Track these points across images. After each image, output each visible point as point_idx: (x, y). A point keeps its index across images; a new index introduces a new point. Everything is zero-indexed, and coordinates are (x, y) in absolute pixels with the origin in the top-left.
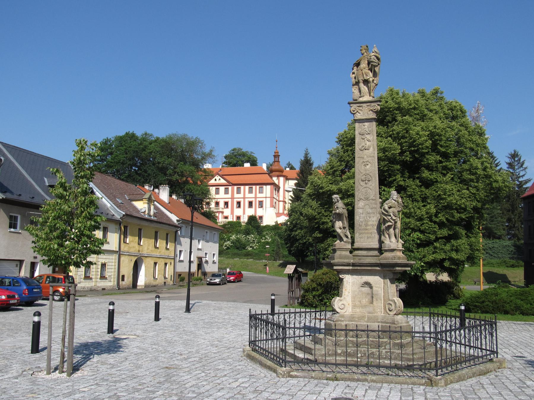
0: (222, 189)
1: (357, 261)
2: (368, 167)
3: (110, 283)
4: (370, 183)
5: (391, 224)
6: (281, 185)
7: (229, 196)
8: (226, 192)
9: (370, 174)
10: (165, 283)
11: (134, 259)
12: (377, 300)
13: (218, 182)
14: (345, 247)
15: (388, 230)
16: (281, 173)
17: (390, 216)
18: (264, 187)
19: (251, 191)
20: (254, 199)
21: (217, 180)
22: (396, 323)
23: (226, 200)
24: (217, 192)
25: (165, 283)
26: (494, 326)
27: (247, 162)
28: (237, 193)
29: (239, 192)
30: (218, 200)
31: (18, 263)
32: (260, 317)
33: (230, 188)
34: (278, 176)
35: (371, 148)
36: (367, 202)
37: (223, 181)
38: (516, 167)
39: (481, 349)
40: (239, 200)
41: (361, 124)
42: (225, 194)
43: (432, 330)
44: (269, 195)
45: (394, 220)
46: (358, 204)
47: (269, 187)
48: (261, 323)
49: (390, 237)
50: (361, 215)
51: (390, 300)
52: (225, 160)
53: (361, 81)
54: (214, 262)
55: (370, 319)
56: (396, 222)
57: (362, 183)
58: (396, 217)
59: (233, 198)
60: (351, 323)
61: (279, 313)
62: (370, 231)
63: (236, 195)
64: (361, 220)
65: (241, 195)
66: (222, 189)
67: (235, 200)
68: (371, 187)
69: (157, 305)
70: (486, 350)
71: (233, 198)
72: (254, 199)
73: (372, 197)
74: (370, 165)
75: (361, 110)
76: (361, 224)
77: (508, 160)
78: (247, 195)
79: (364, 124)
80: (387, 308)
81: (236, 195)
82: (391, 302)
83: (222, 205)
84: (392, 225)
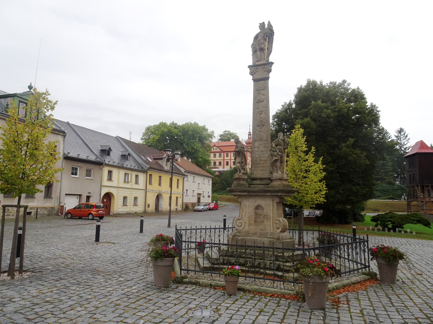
0: (218, 155)
2: (262, 115)
3: (140, 209)
4: (264, 128)
5: (277, 158)
7: (222, 158)
8: (220, 156)
9: (264, 121)
10: (176, 209)
11: (156, 195)
12: (267, 219)
13: (215, 150)
14: (242, 177)
15: (276, 163)
17: (276, 152)
21: (215, 149)
22: (280, 239)
23: (220, 161)
24: (215, 156)
25: (176, 209)
26: (366, 243)
27: (233, 138)
29: (227, 156)
31: (79, 197)
33: (222, 154)
36: (261, 142)
37: (218, 150)
38: (402, 139)
39: (357, 263)
40: (227, 161)
41: (257, 83)
50: (257, 153)
54: (209, 196)
55: (261, 235)
58: (281, 152)
59: (224, 160)
60: (246, 237)
61: (228, 228)
63: (226, 158)
65: (229, 158)
66: (218, 155)
67: (225, 161)
69: (142, 222)
70: (361, 264)
71: (224, 160)
74: (264, 113)
75: (258, 72)
76: (256, 159)
77: (396, 134)
81: (226, 158)
82: (277, 222)
83: (217, 164)
84: (278, 159)
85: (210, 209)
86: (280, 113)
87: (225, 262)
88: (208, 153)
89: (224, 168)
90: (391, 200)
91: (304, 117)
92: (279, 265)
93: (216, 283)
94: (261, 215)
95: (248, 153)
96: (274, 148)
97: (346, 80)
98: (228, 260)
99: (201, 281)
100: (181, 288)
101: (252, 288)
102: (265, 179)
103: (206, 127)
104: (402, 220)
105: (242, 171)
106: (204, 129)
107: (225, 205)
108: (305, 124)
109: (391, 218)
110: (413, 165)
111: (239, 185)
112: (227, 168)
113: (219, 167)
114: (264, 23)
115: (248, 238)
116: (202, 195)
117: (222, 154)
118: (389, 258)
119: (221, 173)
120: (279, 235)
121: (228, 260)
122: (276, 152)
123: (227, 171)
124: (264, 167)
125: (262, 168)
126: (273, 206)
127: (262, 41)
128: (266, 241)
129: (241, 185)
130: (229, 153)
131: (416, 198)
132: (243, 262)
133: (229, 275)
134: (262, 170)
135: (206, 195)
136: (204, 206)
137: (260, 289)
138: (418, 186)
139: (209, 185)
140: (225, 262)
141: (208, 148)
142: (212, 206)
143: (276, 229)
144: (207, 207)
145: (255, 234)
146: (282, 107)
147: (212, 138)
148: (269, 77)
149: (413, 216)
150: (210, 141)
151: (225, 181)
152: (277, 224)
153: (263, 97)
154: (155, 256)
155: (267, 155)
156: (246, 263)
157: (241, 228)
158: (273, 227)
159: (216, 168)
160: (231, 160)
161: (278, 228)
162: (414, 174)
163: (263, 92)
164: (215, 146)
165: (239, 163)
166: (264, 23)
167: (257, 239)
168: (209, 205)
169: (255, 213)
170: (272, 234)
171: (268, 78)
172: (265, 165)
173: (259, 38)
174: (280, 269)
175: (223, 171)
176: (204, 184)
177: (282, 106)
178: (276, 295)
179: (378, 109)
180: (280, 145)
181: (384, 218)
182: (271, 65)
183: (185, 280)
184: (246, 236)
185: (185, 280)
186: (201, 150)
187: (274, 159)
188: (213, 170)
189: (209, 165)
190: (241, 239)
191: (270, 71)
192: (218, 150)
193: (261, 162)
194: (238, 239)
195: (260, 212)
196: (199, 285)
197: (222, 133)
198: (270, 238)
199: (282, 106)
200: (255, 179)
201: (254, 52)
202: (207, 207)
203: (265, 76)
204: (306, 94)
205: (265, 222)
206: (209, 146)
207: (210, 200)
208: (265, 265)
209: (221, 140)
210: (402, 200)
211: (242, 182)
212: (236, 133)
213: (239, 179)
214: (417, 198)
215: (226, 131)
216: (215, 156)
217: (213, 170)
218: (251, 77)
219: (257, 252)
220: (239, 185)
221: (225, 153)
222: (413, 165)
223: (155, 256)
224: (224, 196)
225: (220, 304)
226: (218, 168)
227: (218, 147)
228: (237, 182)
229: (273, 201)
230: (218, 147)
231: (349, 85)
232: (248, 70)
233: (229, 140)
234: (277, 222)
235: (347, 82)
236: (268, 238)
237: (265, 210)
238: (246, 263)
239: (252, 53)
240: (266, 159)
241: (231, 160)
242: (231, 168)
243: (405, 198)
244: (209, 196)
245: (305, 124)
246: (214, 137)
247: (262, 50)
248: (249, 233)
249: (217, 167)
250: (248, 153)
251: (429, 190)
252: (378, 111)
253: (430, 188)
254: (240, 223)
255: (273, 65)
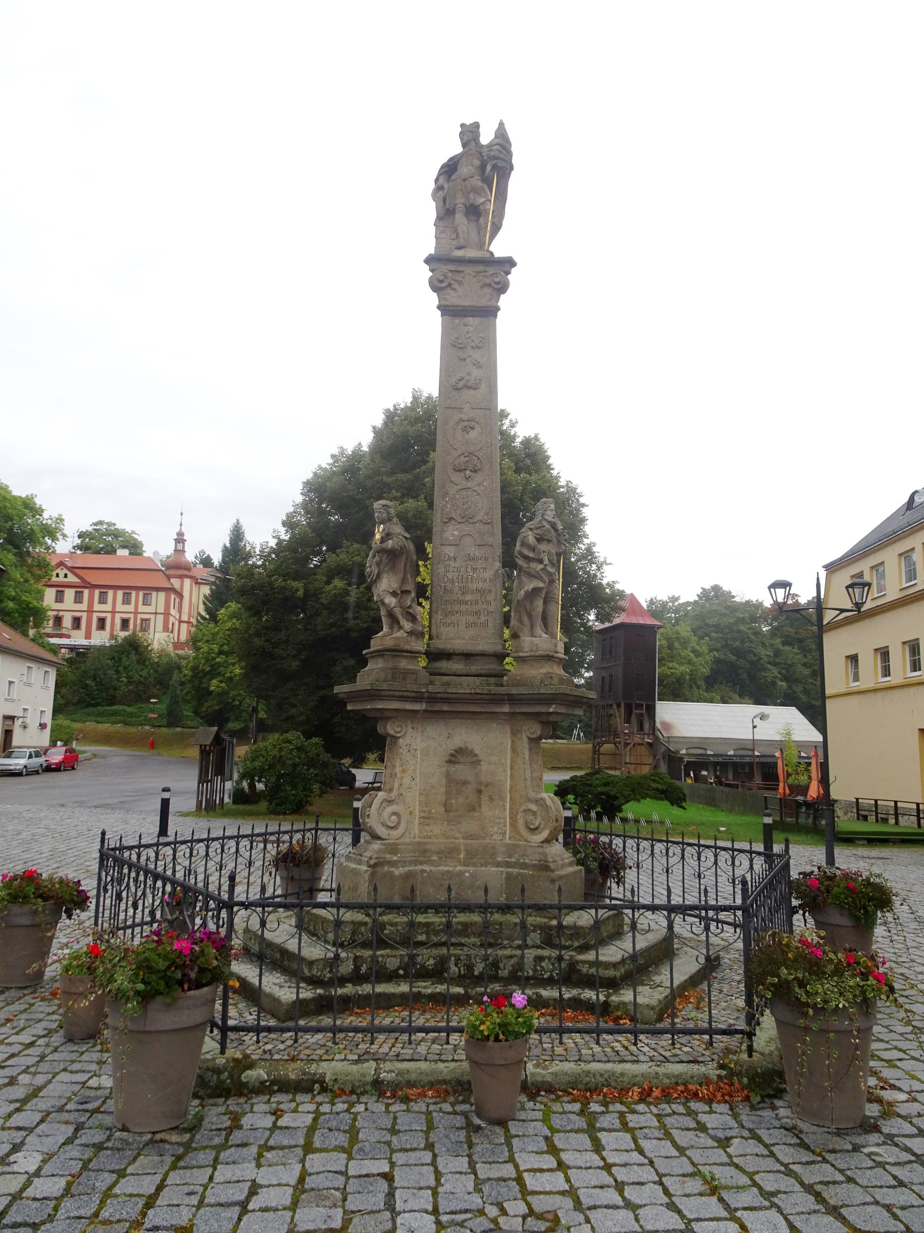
0: (69, 594)
1: (438, 686)
2: (473, 434)
4: (478, 478)
5: (541, 585)
6: (186, 594)
7: (84, 606)
8: (78, 599)
9: (480, 454)
12: (491, 799)
13: (61, 579)
14: (407, 647)
16: (186, 573)
17: (541, 561)
18: (154, 594)
19: (126, 601)
20: (132, 616)
22: (552, 866)
24: (59, 598)
27: (124, 547)
28: (100, 603)
29: (103, 601)
30: (61, 613)
32: (134, 857)
33: (86, 592)
34: (181, 577)
35: (483, 386)
36: (468, 528)
37: (72, 578)
40: (102, 615)
41: (457, 321)
42: (75, 602)
43: (739, 901)
44: (161, 609)
45: (550, 574)
46: (443, 532)
47: (162, 595)
48: (136, 880)
49: (532, 626)
50: (452, 563)
51: (529, 800)
52: (79, 541)
53: (460, 207)
54: (43, 726)
56: (552, 582)
57: (457, 477)
59: (90, 611)
60: (419, 868)
62: (475, 608)
64: (450, 575)
65: (108, 607)
66: (69, 594)
67: (95, 615)
68: (479, 489)
71: (90, 611)
72: (132, 616)
73: (481, 516)
74: (478, 429)
75: (460, 283)
76: (449, 586)
78: (120, 607)
79: (466, 320)
80: (520, 822)
81: (97, 607)
82: (533, 807)
83: (67, 622)
84: (542, 588)
85: (49, 769)
86: (329, 479)
87: (364, 969)
88: (40, 586)
89: (88, 636)
90: (551, 741)
91: (403, 495)
92: (573, 965)
93: (400, 1073)
94: (465, 783)
95: (173, 596)
96: (533, 549)
97: (508, 410)
98: (374, 958)
99: (328, 1069)
100: (257, 1117)
101: (555, 1074)
102: (483, 655)
103: (38, 501)
104: (633, 791)
105: (407, 625)
106: (29, 506)
107: (95, 756)
108: (410, 515)
109: (606, 784)
110: (611, 653)
111: (396, 674)
112: (100, 639)
113: (74, 633)
114: (476, 125)
115: (426, 868)
116: (18, 723)
117: (86, 592)
118: (864, 907)
119: (78, 654)
120: (545, 854)
121: (374, 958)
122: (541, 561)
123: (101, 649)
124: (477, 613)
125: (471, 619)
126: (514, 750)
127: (477, 182)
128: (493, 876)
129: (406, 673)
130: (111, 593)
131: (612, 733)
132: (432, 962)
133: (497, 1039)
134: (469, 625)
135: (33, 721)
136: (30, 757)
137: (588, 1073)
138: (619, 705)
139: (47, 688)
140: (364, 969)
141: (41, 569)
142: (57, 755)
143: (525, 833)
144: (41, 760)
145: (450, 853)
146: (331, 461)
147: (54, 539)
148: (498, 309)
149: (654, 781)
150: (48, 548)
151: (94, 678)
152: (534, 813)
153: (476, 373)
154: (140, 987)
155: (489, 574)
156: (442, 963)
157: (395, 833)
158: (514, 825)
159: (61, 636)
160: (113, 612)
161: (534, 830)
162: (611, 676)
163: (476, 355)
164: (61, 564)
165: (394, 594)
166: (476, 125)
167: (460, 874)
168: (45, 754)
169: (448, 775)
170: (511, 850)
171: (491, 312)
172: (480, 607)
173: (464, 170)
174: (575, 977)
175: (88, 648)
176: (29, 685)
177: (333, 456)
178: (656, 1093)
179: (582, 500)
180: (549, 541)
181: (590, 786)
182: (506, 269)
183: (250, 1075)
184: (416, 863)
185: (250, 1075)
186: (16, 574)
187: (531, 586)
188: (53, 641)
189: (37, 625)
190: (401, 875)
191: (503, 288)
192: (72, 578)
193: (468, 597)
194: (392, 873)
195: (462, 771)
196: (324, 1089)
197: (87, 527)
198: (508, 865)
199: (333, 456)
200: (447, 655)
201: (445, 214)
202: (41, 760)
203: (484, 302)
204: (411, 430)
205: (485, 809)
206: (43, 565)
207: (44, 740)
208: (520, 966)
209: (84, 548)
210: (574, 739)
211: (404, 664)
212: (133, 532)
213: (395, 652)
214: (616, 735)
215: (101, 523)
216: (59, 598)
217: (53, 641)
218: (434, 298)
219: (530, 920)
220: (396, 674)
221: (97, 592)
222: (611, 653)
223: (140, 987)
224: (90, 726)
225: (84, 1083)
226: (68, 637)
227: (72, 569)
228: (390, 664)
229: (514, 734)
230: (72, 569)
231: (513, 425)
232: (426, 273)
233: (110, 551)
234: (533, 807)
235: (509, 417)
236: (498, 865)
237: (484, 767)
238: (442, 963)
239: (435, 215)
240: (486, 586)
241: (113, 612)
242: (113, 637)
243: (579, 735)
244: (43, 726)
245: (410, 515)
246: (64, 536)
247: (474, 212)
248: (425, 851)
249: (64, 631)
250: (173, 596)
251: (642, 715)
252: (583, 505)
253: (644, 711)
254: (394, 813)
255: (513, 270)
